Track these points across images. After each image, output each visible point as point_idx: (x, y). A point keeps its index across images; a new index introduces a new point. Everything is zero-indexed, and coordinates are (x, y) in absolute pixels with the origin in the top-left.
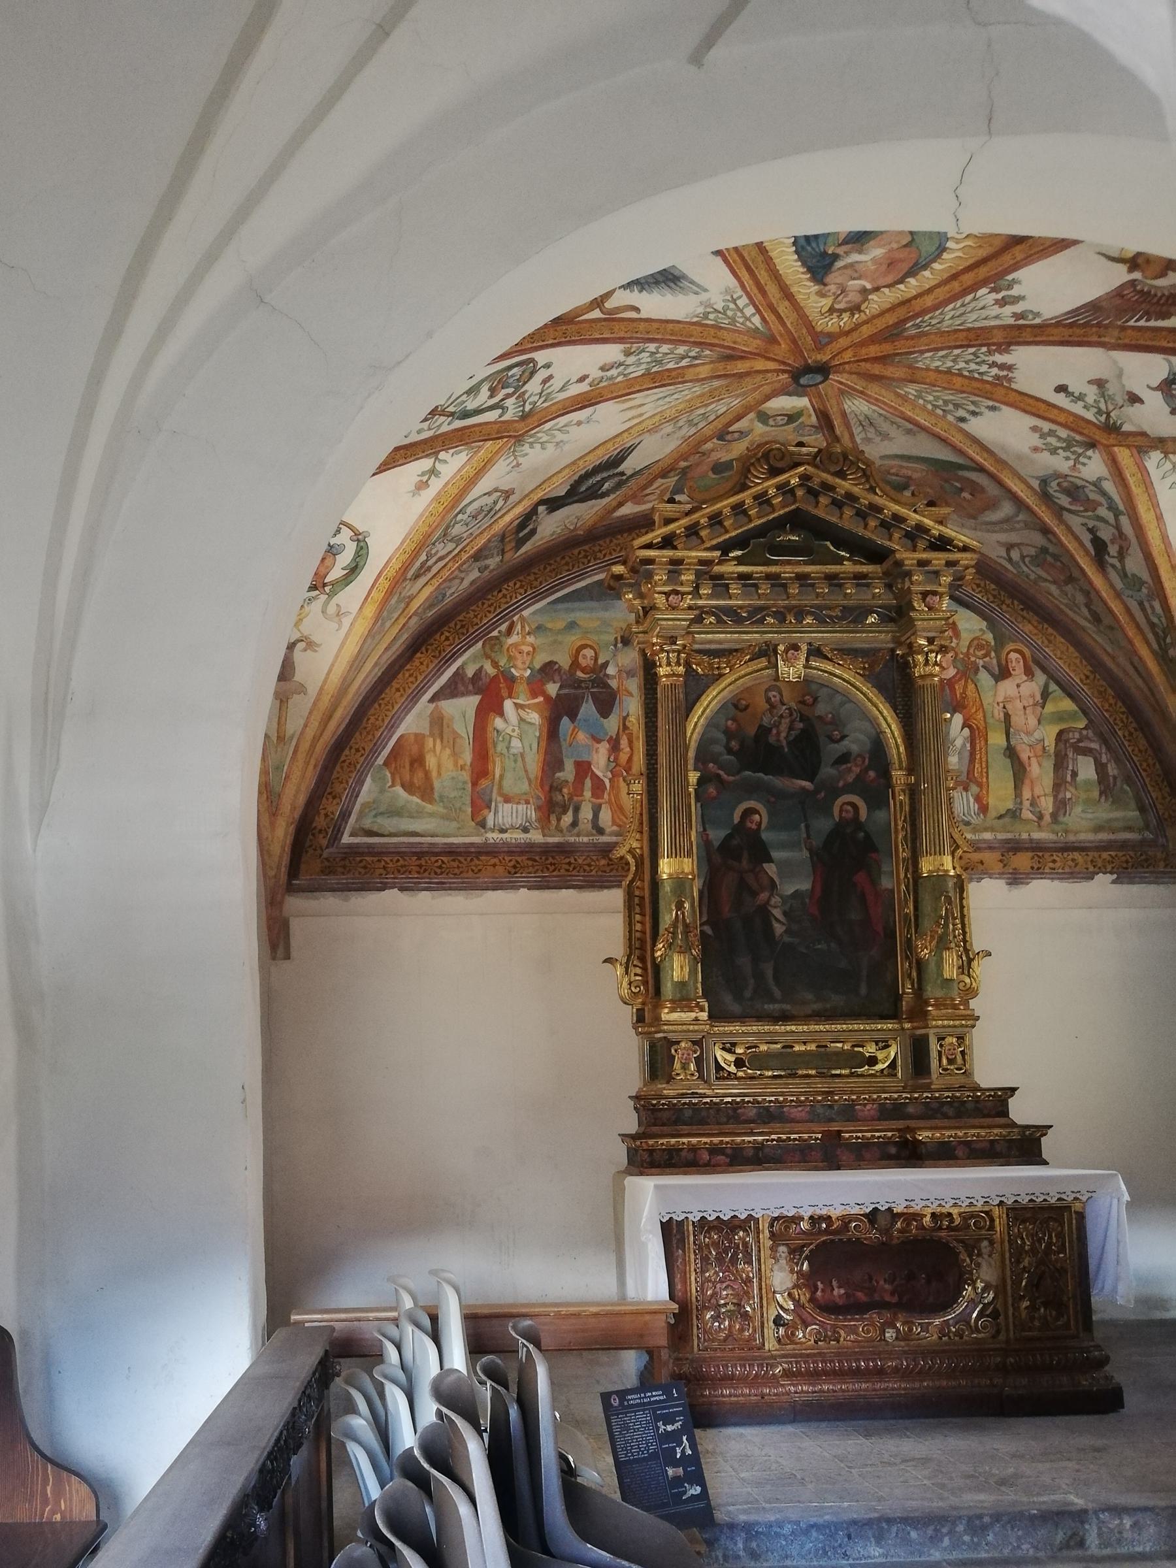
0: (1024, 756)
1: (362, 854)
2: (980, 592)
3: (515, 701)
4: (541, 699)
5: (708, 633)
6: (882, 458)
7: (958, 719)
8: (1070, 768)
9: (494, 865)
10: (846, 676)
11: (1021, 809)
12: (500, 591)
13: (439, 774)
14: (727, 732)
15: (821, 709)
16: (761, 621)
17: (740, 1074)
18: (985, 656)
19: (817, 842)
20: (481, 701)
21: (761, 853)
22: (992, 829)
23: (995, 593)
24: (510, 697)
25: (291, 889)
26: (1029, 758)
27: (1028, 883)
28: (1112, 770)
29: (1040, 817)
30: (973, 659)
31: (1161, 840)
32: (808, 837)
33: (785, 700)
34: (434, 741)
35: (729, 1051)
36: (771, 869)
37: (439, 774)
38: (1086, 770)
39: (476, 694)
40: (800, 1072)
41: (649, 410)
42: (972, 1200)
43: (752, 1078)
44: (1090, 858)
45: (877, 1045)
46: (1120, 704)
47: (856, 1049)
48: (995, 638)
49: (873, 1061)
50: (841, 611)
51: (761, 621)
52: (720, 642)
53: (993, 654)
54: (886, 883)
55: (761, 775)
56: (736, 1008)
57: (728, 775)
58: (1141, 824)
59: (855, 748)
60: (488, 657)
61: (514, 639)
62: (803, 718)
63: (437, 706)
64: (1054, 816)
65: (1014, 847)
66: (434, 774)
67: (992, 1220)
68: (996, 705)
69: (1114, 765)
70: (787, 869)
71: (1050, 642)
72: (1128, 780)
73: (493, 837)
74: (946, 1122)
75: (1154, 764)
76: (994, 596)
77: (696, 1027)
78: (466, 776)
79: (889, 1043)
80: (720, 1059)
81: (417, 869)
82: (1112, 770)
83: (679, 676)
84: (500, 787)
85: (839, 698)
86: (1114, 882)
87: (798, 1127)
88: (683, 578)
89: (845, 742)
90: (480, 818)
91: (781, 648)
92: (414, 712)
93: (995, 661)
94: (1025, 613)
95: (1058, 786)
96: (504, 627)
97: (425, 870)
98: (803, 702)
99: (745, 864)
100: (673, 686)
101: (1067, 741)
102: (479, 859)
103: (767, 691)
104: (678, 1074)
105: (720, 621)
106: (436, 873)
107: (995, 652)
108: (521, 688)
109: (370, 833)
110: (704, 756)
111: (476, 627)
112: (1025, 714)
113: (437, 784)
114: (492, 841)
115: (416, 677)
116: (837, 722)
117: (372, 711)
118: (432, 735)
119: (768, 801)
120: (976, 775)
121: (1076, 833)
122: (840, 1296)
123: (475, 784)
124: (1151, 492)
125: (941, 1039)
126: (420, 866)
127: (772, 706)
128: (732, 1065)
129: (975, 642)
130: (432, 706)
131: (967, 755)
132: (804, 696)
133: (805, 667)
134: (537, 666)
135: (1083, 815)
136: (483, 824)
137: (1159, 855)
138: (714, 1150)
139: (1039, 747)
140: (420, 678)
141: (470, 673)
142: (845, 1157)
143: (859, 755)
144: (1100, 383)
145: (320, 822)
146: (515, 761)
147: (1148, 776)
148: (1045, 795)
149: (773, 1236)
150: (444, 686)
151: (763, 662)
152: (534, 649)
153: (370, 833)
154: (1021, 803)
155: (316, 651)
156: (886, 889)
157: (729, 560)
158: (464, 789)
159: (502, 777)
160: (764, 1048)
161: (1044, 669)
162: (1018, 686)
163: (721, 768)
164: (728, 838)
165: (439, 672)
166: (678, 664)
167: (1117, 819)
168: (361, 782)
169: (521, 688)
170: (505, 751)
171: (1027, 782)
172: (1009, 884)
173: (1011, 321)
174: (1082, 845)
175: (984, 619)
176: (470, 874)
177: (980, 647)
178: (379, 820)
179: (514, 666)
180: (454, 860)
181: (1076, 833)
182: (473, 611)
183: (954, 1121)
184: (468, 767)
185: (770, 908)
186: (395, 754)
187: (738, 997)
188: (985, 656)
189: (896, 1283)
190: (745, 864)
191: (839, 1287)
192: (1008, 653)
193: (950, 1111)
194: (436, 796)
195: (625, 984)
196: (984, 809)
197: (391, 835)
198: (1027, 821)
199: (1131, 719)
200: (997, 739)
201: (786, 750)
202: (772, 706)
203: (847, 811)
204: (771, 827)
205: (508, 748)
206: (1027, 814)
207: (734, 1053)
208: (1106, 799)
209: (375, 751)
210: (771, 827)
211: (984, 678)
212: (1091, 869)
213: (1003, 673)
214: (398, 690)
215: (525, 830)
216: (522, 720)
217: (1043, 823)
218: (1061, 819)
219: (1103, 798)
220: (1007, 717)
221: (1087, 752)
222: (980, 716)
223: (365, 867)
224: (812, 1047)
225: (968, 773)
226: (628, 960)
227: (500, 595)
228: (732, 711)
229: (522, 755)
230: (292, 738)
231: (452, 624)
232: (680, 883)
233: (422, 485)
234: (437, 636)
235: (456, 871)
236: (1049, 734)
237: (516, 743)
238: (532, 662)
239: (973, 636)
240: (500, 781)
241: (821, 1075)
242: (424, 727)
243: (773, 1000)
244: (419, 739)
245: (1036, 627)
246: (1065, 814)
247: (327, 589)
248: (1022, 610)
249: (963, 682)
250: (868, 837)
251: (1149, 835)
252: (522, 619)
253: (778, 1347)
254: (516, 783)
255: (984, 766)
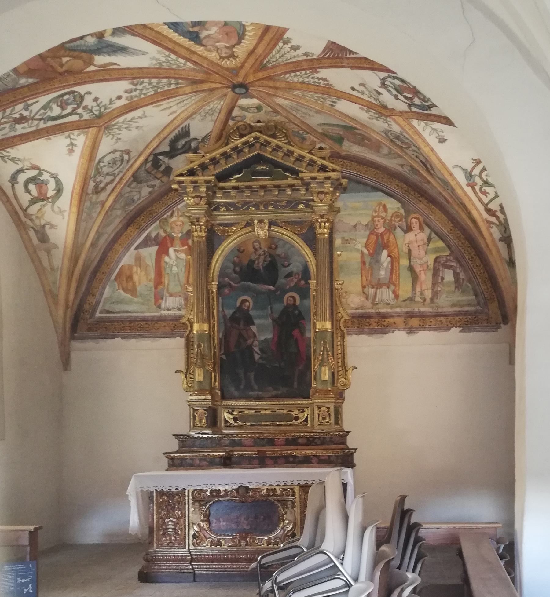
0: (418, 269)
1: (104, 322)
2: (398, 189)
3: (175, 248)
4: (186, 247)
5: (222, 215)
6: (320, 125)
7: (385, 253)
8: (441, 275)
9: (165, 326)
10: (289, 235)
11: (415, 297)
12: (168, 196)
13: (140, 283)
14: (234, 263)
15: (279, 251)
16: (247, 209)
17: (236, 424)
18: (399, 221)
19: (276, 316)
20: (159, 248)
21: (249, 321)
22: (400, 307)
23: (406, 189)
24: (172, 246)
25: (73, 338)
26: (420, 271)
27: (417, 333)
28: (462, 276)
29: (425, 300)
30: (393, 222)
31: (486, 310)
32: (272, 313)
33: (263, 247)
34: (137, 268)
35: (231, 414)
36: (254, 328)
37: (140, 283)
38: (449, 276)
39: (157, 245)
40: (263, 423)
41: (178, 109)
42: (272, 483)
43: (242, 426)
44: (449, 320)
45: (299, 411)
46: (467, 243)
47: (289, 413)
48: (405, 212)
49: (297, 418)
50: (286, 203)
51: (247, 209)
52: (228, 219)
53: (404, 220)
54: (307, 335)
55: (250, 283)
56: (236, 394)
57: (235, 284)
58: (476, 302)
59: (295, 270)
60: (161, 228)
61: (174, 219)
62: (270, 255)
63: (138, 252)
64: (432, 299)
65: (411, 315)
66: (137, 284)
67: (294, 492)
68: (404, 245)
69: (463, 274)
70: (261, 328)
71: (432, 212)
72: (470, 281)
73: (165, 313)
74: (316, 447)
75: (484, 272)
76: (405, 191)
77: (205, 403)
78: (152, 284)
79: (305, 410)
80: (226, 418)
81: (129, 328)
82: (462, 276)
83: (202, 237)
84: (168, 290)
85: (287, 246)
86: (460, 331)
87: (247, 448)
88: (201, 189)
89: (291, 267)
90: (158, 304)
91: (256, 222)
92: (128, 254)
93: (404, 224)
94: (420, 199)
95: (434, 284)
96: (169, 213)
97: (133, 329)
98: (270, 248)
99: (242, 326)
100: (198, 242)
101: (439, 262)
102: (157, 323)
103: (254, 242)
104: (197, 424)
105: (228, 210)
106: (138, 330)
107: (405, 219)
108: (177, 242)
109: (108, 312)
110: (223, 274)
111: (156, 214)
112: (419, 249)
113: (138, 288)
114: (164, 315)
115: (129, 238)
116: (286, 258)
117: (109, 255)
118: (136, 266)
119: (253, 296)
120: (393, 280)
121: (443, 307)
122: (223, 526)
123: (156, 288)
124: (422, 137)
125: (319, 408)
126: (131, 327)
127: (256, 250)
128: (232, 420)
129: (395, 215)
130: (136, 251)
131: (389, 270)
132: (271, 244)
133: (269, 231)
134: (185, 231)
135: (447, 299)
136: (159, 307)
137: (485, 318)
138: (202, 459)
139: (425, 266)
140: (130, 239)
141: (153, 235)
142: (269, 462)
143: (296, 273)
144: (362, 85)
145: (87, 307)
146: (175, 277)
147: (480, 278)
148: (428, 289)
149: (193, 498)
150: (141, 242)
151: (249, 229)
152: (183, 223)
153: (108, 312)
154: (415, 294)
155: (56, 229)
156: (308, 338)
157: (232, 180)
158: (151, 290)
159: (168, 284)
160: (246, 412)
161: (429, 227)
162: (416, 235)
163: (231, 280)
164: (234, 314)
165: (139, 236)
166: (201, 231)
167: (462, 301)
168: (104, 288)
169: (177, 242)
170: (169, 272)
171: (419, 283)
172: (407, 333)
173: (305, 57)
174: (445, 313)
175: (400, 202)
176: (154, 330)
177: (397, 216)
178: (113, 305)
179: (174, 232)
180: (146, 324)
181: (443, 307)
182: (155, 206)
183: (320, 446)
184: (153, 280)
185: (253, 347)
186: (119, 275)
187: (237, 388)
188: (399, 221)
189: (249, 520)
190: (242, 326)
191: (224, 521)
192: (412, 219)
193: (318, 442)
194: (138, 294)
195: (185, 383)
196: (397, 297)
197: (118, 312)
198: (418, 302)
199: (473, 250)
200: (404, 262)
201: (262, 271)
202: (256, 250)
203: (290, 300)
204: (254, 308)
205: (171, 271)
206: (418, 299)
207: (233, 414)
208: (459, 290)
209: (110, 274)
210: (254, 308)
211: (399, 232)
212: (450, 325)
213: (408, 229)
214: (120, 245)
215: (179, 309)
216: (177, 257)
217: (426, 303)
218: (435, 301)
219: (457, 289)
220: (410, 251)
221: (450, 267)
222: (396, 251)
223: (106, 328)
224: (269, 412)
225: (390, 279)
226: (187, 370)
227: (168, 198)
228: (237, 253)
229: (178, 274)
230: (58, 268)
231: (145, 213)
232: (201, 335)
233: (71, 151)
234: (138, 219)
235: (148, 329)
236: (430, 259)
237: (175, 269)
238: (182, 229)
239: (394, 211)
240: (168, 287)
241: (273, 425)
242: (132, 262)
243: (253, 390)
244: (130, 267)
245: (426, 205)
246: (437, 298)
247: (50, 200)
248: (419, 197)
249: (388, 234)
250: (300, 313)
251: (479, 308)
252: (178, 209)
253: (194, 548)
254: (174, 288)
255: (397, 275)
